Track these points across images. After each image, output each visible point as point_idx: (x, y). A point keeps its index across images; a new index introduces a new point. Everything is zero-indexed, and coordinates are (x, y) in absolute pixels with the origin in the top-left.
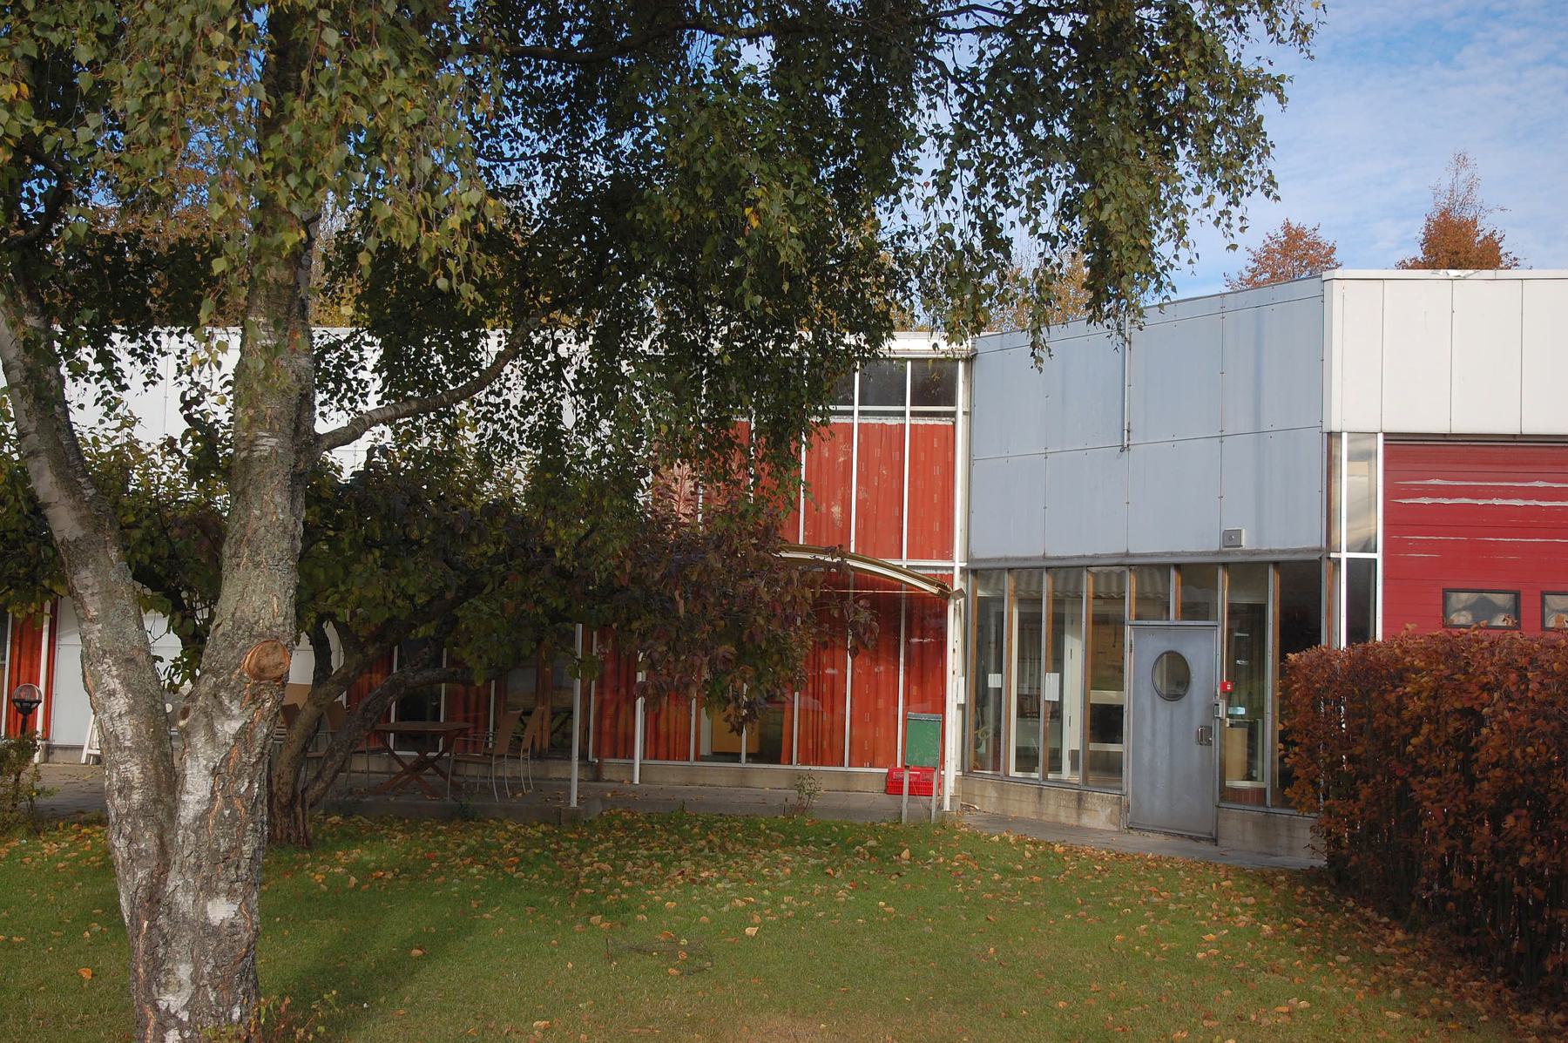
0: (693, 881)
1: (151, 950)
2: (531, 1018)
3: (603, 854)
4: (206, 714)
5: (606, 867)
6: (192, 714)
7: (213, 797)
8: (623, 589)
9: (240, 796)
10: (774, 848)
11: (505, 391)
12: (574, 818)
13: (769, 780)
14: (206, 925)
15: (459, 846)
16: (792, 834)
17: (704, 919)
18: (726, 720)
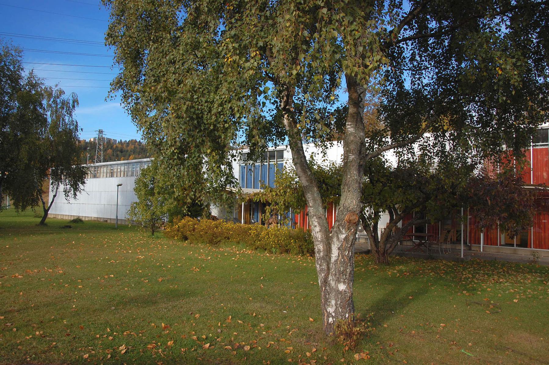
0: (497, 282)
1: (325, 295)
2: (440, 322)
3: (469, 271)
4: (337, 233)
5: (470, 276)
6: (333, 232)
7: (339, 256)
8: (471, 197)
9: (346, 256)
10: (525, 273)
11: (429, 141)
12: (462, 261)
13: (524, 253)
14: (338, 290)
15: (428, 267)
16: (531, 270)
17: (500, 295)
18: (508, 235)
